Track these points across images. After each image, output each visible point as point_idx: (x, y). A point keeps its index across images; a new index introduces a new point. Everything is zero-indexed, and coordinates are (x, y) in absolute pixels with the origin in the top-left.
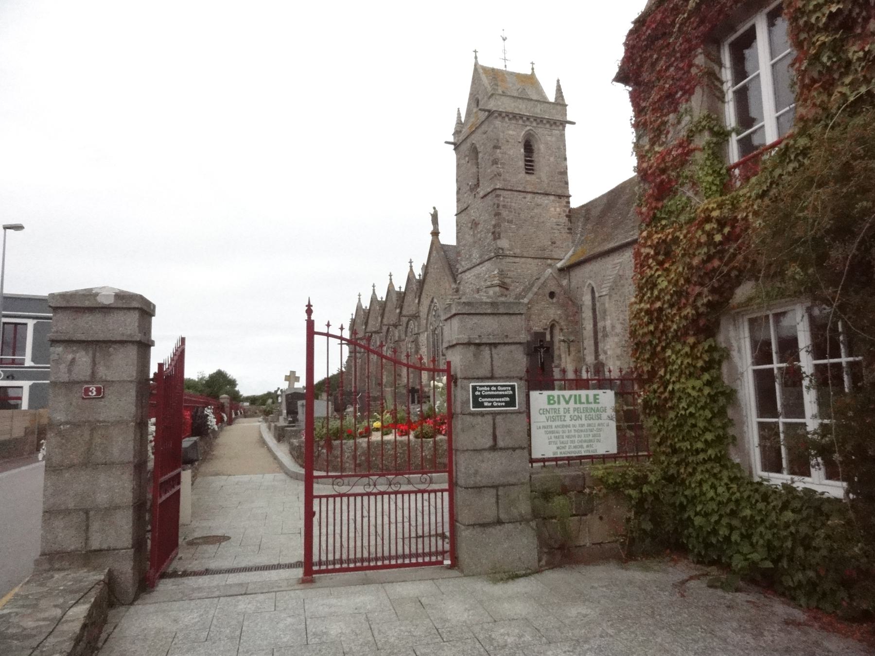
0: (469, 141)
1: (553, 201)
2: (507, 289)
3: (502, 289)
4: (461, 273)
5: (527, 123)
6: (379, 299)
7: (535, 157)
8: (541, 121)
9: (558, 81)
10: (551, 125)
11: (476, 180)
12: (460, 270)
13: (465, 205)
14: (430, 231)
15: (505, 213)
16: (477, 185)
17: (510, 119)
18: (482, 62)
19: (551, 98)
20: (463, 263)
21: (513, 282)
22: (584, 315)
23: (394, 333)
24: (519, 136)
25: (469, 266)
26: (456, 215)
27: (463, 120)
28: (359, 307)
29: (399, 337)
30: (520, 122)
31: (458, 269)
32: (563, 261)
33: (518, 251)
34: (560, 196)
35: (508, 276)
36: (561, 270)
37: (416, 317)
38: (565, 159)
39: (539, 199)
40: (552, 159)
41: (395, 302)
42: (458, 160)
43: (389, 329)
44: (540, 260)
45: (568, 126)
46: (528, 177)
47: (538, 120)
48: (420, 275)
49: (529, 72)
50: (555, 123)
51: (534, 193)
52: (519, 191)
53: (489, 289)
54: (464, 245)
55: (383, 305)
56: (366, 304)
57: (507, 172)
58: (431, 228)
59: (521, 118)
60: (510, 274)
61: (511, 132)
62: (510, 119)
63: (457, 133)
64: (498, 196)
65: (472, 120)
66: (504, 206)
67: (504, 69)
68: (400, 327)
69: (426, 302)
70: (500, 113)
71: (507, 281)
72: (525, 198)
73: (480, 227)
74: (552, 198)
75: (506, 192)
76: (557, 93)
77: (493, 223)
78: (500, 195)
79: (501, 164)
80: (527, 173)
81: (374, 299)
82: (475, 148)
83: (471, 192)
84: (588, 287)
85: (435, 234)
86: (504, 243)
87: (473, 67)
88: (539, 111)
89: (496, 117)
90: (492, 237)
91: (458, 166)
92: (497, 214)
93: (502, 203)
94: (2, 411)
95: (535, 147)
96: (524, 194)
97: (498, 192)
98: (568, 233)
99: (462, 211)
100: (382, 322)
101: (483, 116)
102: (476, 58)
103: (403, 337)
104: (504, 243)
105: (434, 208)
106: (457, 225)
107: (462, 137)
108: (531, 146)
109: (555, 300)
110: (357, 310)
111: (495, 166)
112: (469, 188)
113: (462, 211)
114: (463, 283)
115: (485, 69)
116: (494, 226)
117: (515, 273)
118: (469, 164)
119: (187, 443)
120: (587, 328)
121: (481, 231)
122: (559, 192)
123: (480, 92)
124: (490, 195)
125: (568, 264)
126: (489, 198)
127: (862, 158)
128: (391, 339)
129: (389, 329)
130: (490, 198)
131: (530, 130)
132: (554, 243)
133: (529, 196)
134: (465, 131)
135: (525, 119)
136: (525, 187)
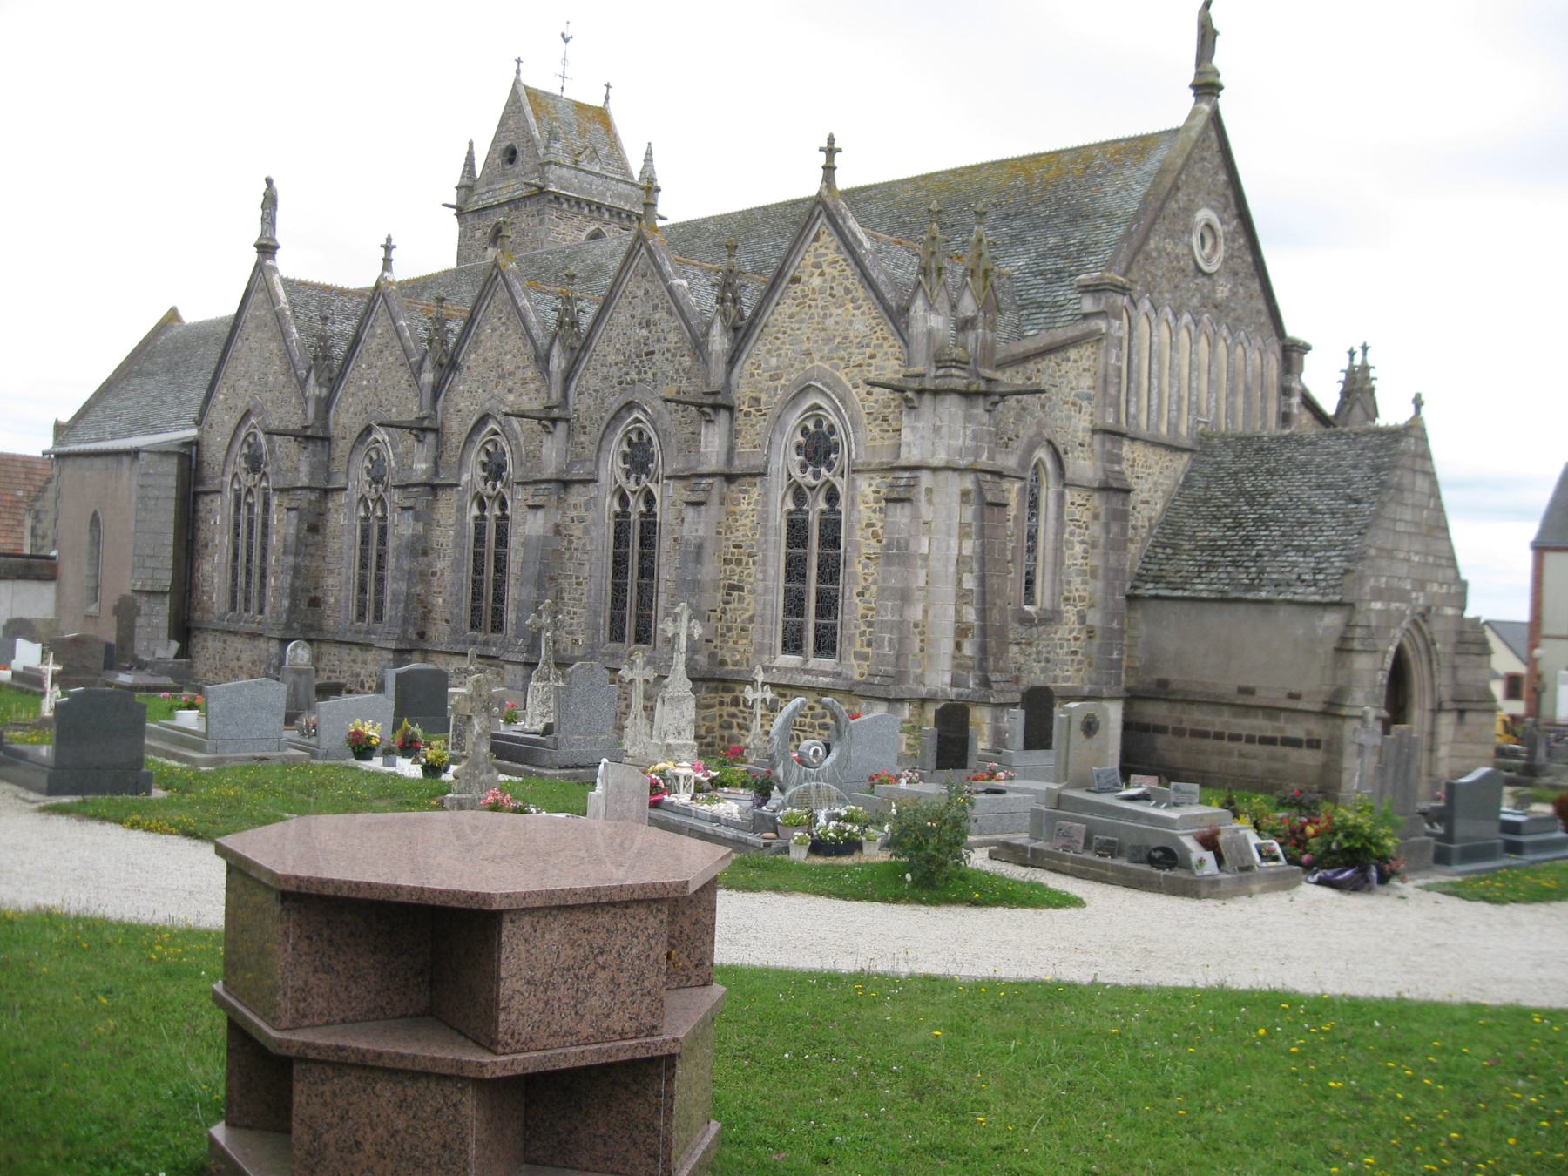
18: (529, 80)
19: (636, 167)
49: (599, 103)
58: (255, 232)
67: (558, 93)
87: (510, 87)
94: (1558, 1004)
102: (518, 72)
115: (534, 95)
127: (1345, 1121)
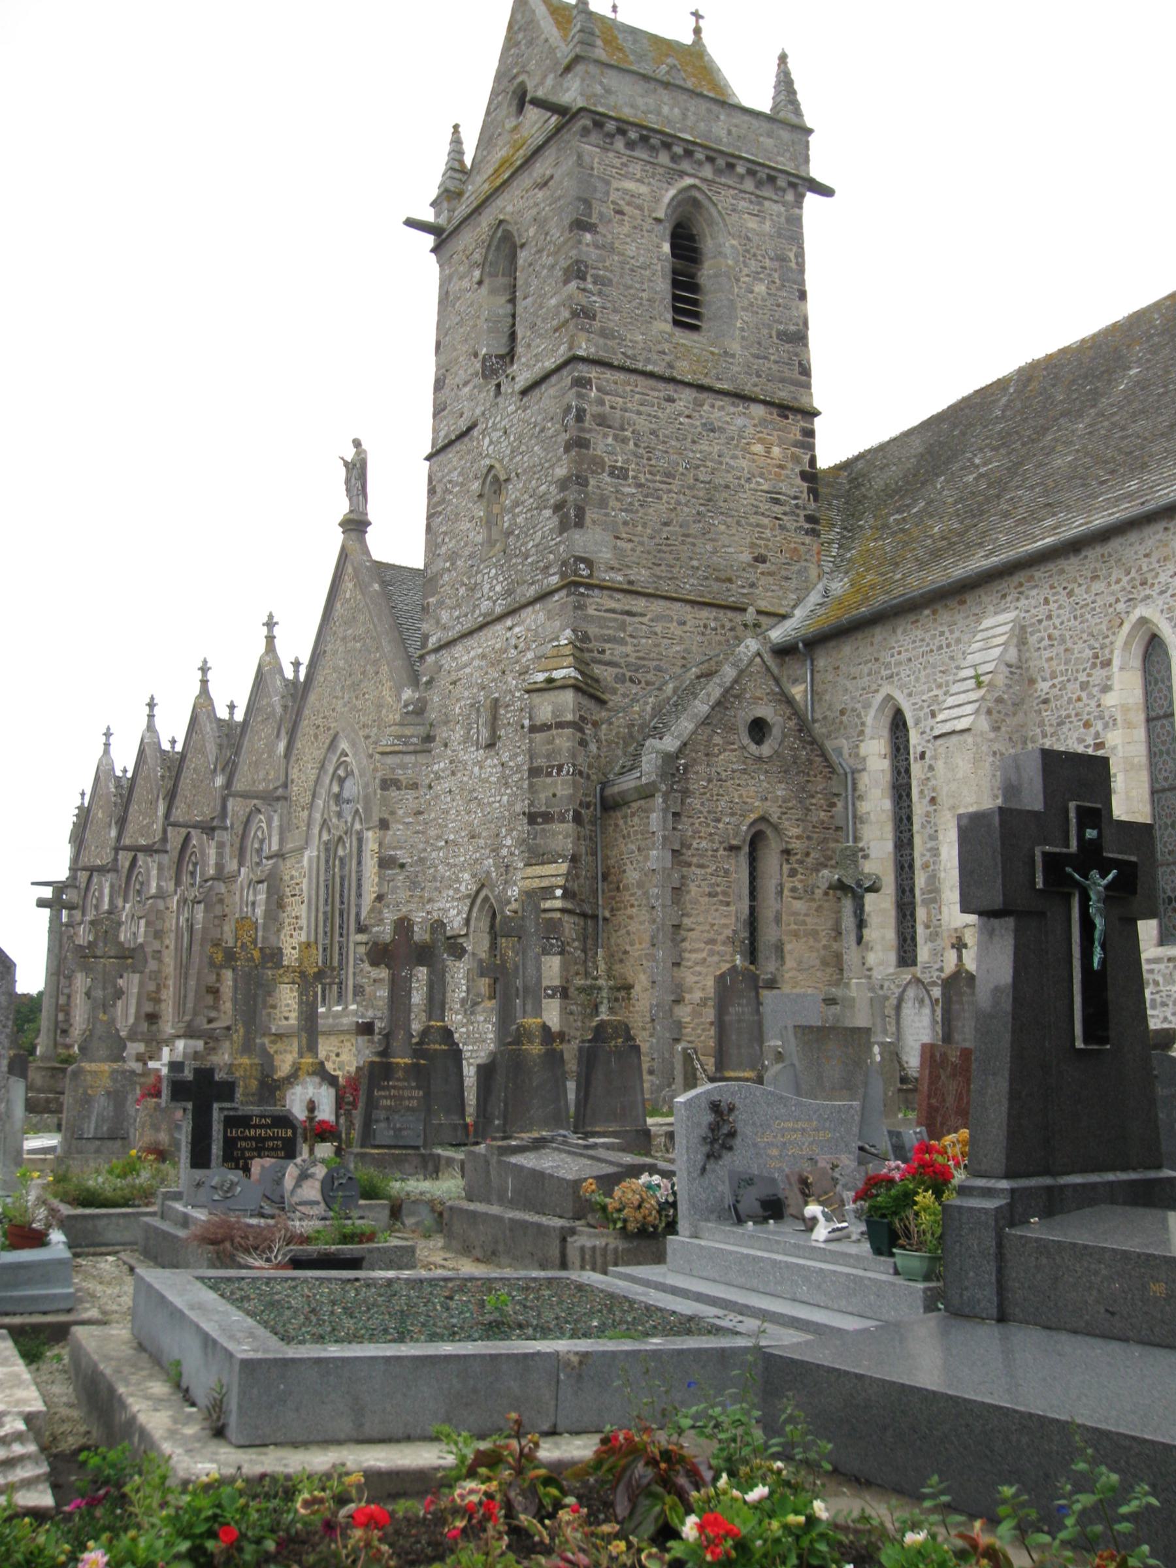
0: (486, 221)
1: (763, 422)
2: (602, 702)
3: (586, 702)
4: (437, 650)
5: (686, 166)
6: (166, 746)
7: (706, 274)
8: (731, 167)
9: (783, 58)
10: (759, 184)
11: (504, 340)
12: (432, 642)
13: (463, 425)
14: (340, 518)
15: (602, 444)
16: (510, 356)
17: (630, 145)
20: (445, 616)
21: (620, 679)
22: (864, 807)
23: (203, 853)
24: (657, 200)
25: (468, 624)
26: (429, 458)
27: (468, 161)
28: (104, 772)
29: (220, 867)
30: (664, 158)
31: (426, 637)
32: (789, 624)
33: (642, 576)
34: (784, 409)
35: (607, 656)
36: (784, 652)
37: (277, 797)
38: (803, 295)
39: (718, 412)
40: (760, 288)
41: (211, 749)
42: (445, 282)
43: (187, 838)
44: (714, 613)
45: (811, 199)
46: (683, 338)
47: (721, 162)
48: (296, 664)
49: (687, 39)
50: (772, 179)
51: (701, 388)
52: (651, 375)
53: (537, 698)
54: (453, 557)
55: (175, 765)
56: (125, 760)
57: (615, 311)
58: (342, 507)
59: (667, 146)
60: (614, 652)
61: (630, 185)
62: (630, 145)
63: (448, 196)
64: (581, 383)
65: (500, 153)
66: (602, 421)
67: (611, 15)
68: (225, 837)
69: (310, 750)
70: (599, 121)
71: (606, 674)
72: (670, 400)
73: (512, 492)
74: (758, 411)
75: (609, 374)
76: (777, 93)
77: (561, 472)
78: (589, 381)
79: (597, 280)
80: (676, 323)
81: (148, 749)
82: (507, 237)
83: (484, 376)
84: (881, 708)
85: (356, 525)
86: (587, 541)
88: (723, 134)
89: (585, 132)
90: (555, 520)
91: (445, 300)
92: (579, 443)
93: (591, 409)
95: (708, 246)
96: (670, 389)
97: (583, 370)
98: (808, 532)
99: (451, 443)
100: (167, 815)
101: (535, 122)
103: (232, 865)
104: (587, 541)
105: (357, 443)
106: (432, 491)
107: (462, 209)
108: (692, 238)
109: (766, 750)
110: (97, 779)
111: (573, 285)
112: (478, 366)
113: (451, 443)
114: (443, 682)
116: (563, 485)
117: (629, 649)
118: (484, 290)
119: (967, 1149)
120: (873, 853)
121: (517, 504)
122: (783, 394)
123: (532, 66)
124: (554, 379)
125: (812, 629)
126: (549, 391)
128: (193, 874)
129: (187, 838)
130: (552, 391)
131: (693, 186)
132: (760, 559)
133: (688, 395)
134: (476, 188)
135: (678, 150)
136: (670, 366)
